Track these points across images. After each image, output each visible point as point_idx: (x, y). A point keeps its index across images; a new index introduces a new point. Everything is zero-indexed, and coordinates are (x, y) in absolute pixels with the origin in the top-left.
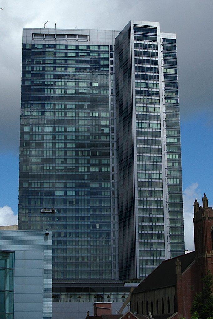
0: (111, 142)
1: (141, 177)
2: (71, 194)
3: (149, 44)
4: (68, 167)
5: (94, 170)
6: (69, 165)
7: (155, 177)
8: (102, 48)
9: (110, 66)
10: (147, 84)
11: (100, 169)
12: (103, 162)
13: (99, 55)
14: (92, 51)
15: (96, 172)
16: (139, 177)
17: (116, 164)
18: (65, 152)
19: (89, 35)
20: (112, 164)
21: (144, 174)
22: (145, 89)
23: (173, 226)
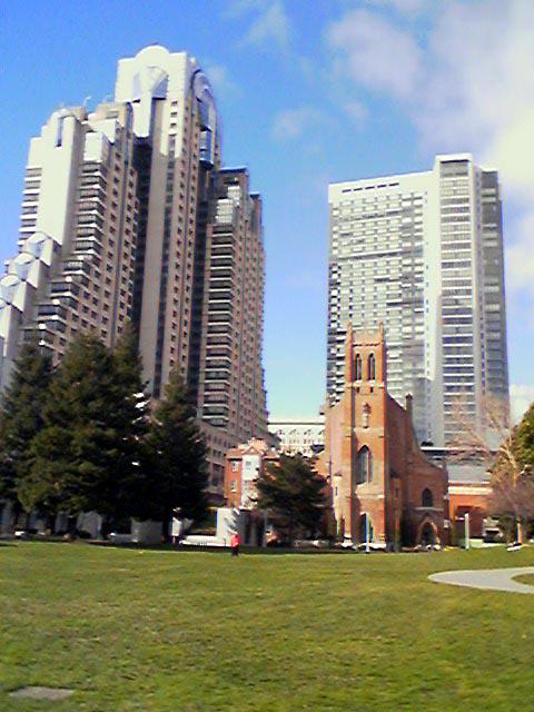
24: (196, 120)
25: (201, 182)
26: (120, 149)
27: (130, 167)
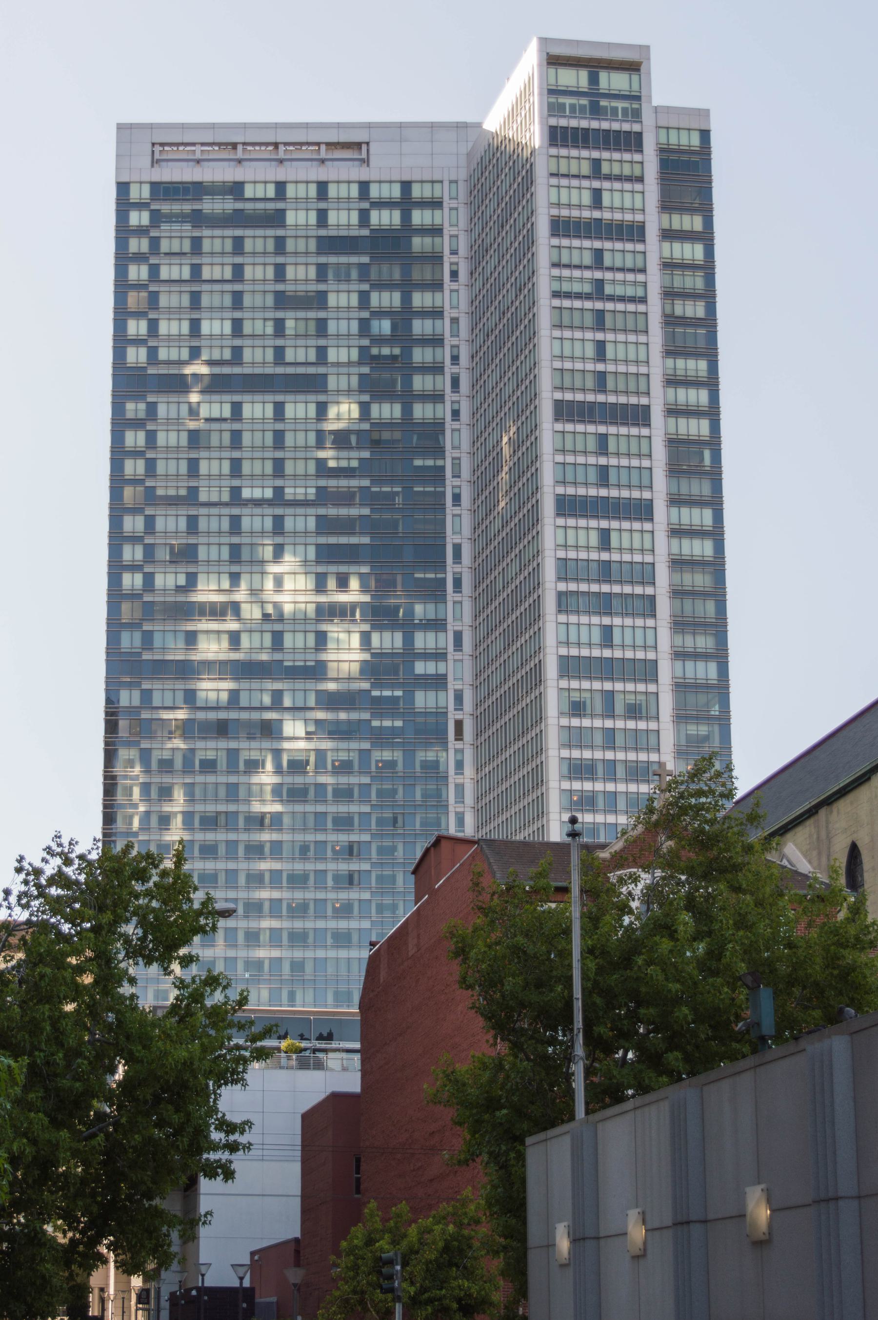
0: (453, 716)
1: (571, 541)
2: (302, 220)
3: (615, 401)
4: (286, 664)
5: (387, 644)
6: (291, 657)
7: (626, 544)
8: (416, 192)
9: (449, 369)
10: (603, 439)
11: (407, 410)
12: (416, 275)
13: (406, 217)
14: (381, 204)
15: (390, 425)
16: (564, 640)
17: (467, 618)
18: (279, 436)
19: (368, 143)
20: (451, 336)
21: (578, 345)
22: (590, 398)
23: (694, 727)
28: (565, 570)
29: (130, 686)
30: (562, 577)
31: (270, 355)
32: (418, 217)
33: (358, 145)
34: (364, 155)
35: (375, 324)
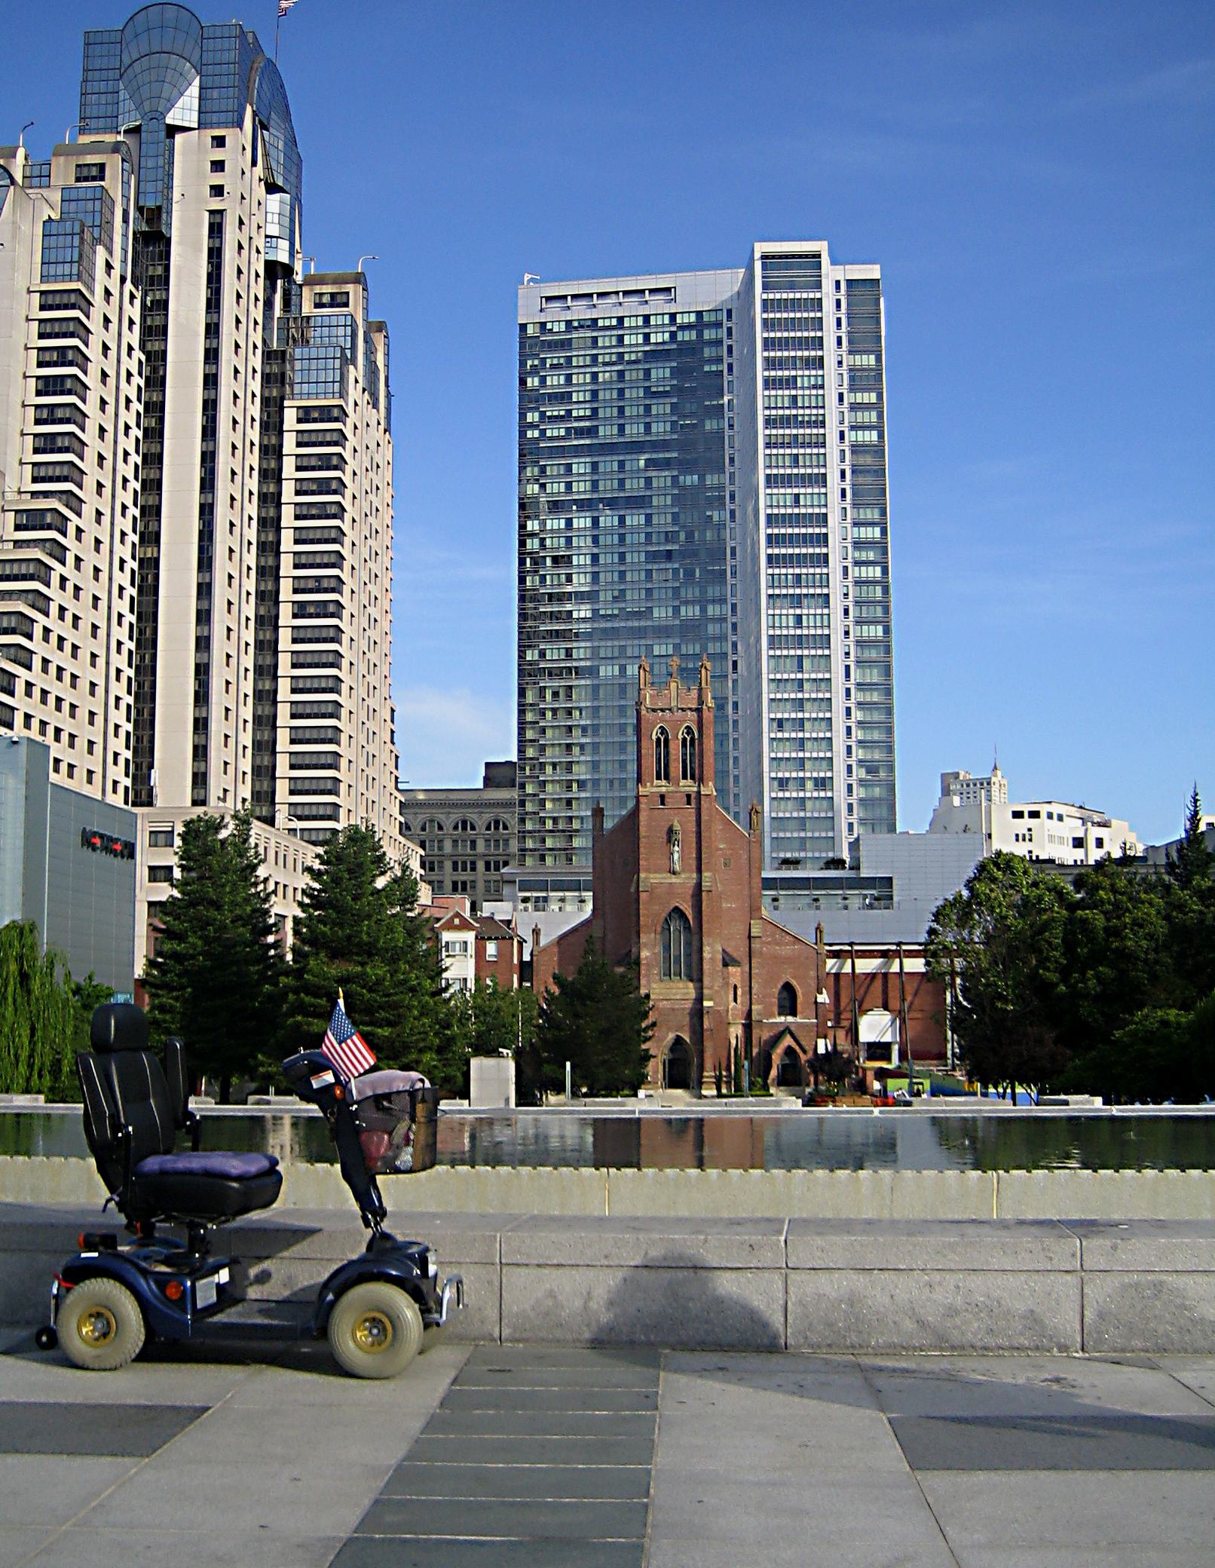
13: (703, 610)
14: (683, 328)
24: (259, 170)
25: (269, 304)
26: (111, 253)
27: (129, 286)
28: (769, 422)
29: (531, 409)
30: (765, 310)
31: (615, 431)
32: (708, 334)
33: (668, 290)
34: (673, 296)
35: (683, 609)
